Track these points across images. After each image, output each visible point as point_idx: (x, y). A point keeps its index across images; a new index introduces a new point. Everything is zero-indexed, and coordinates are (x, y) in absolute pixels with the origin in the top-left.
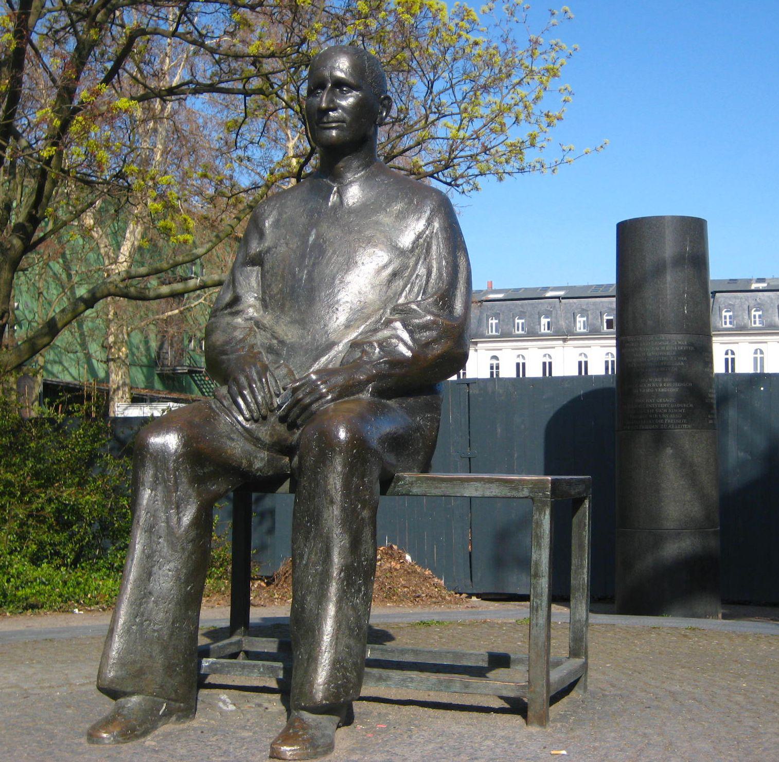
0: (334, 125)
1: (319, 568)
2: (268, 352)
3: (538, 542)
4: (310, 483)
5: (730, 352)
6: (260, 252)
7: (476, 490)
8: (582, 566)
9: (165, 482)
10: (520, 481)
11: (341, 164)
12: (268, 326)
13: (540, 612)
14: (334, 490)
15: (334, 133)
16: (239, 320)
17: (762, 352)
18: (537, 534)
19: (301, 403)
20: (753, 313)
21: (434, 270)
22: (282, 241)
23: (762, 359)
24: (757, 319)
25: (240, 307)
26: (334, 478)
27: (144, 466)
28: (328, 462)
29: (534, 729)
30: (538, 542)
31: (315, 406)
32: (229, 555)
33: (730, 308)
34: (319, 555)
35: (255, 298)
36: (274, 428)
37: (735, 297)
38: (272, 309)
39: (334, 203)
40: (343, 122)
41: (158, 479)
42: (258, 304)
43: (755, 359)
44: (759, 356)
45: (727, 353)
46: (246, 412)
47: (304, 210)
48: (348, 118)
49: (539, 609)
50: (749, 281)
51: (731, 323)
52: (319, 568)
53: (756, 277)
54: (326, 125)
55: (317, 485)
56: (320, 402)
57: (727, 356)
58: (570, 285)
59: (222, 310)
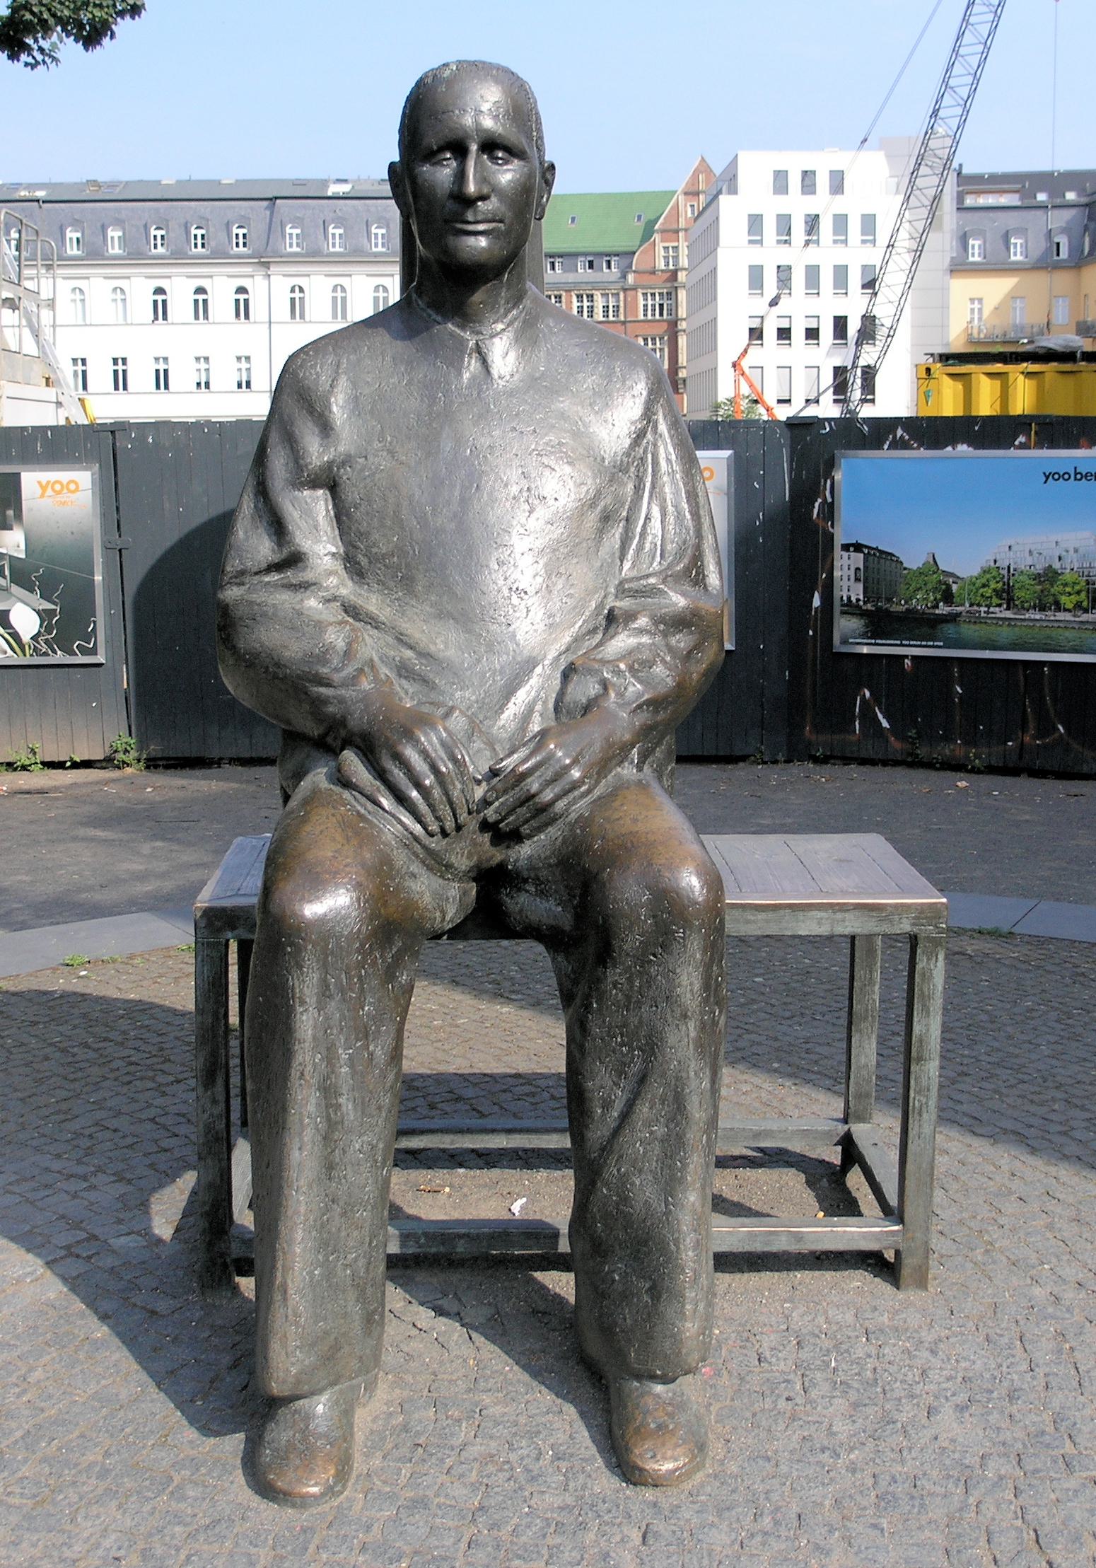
0: (481, 227)
1: (659, 1130)
2: (400, 676)
3: (924, 1005)
4: (630, 980)
5: (297, 289)
6: (330, 464)
7: (819, 923)
8: (871, 982)
9: (343, 992)
10: (896, 906)
11: (478, 297)
12: (382, 618)
13: (925, 1115)
14: (689, 995)
15: (483, 242)
16: (312, 603)
17: (343, 289)
18: (923, 993)
19: (537, 800)
20: (331, 230)
21: (670, 509)
22: (376, 445)
23: (344, 299)
24: (337, 241)
25: (308, 576)
26: (689, 974)
27: (300, 967)
28: (675, 946)
29: (909, 1295)
30: (924, 1005)
31: (560, 805)
32: (192, 969)
33: (297, 222)
34: (659, 1106)
35: (333, 555)
36: (474, 844)
37: (304, 207)
38: (379, 582)
39: (473, 378)
40: (501, 221)
41: (327, 987)
42: (338, 566)
43: (334, 299)
44: (339, 294)
45: (293, 291)
46: (429, 818)
47: (410, 383)
48: (509, 215)
49: (924, 1110)
50: (325, 183)
51: (298, 245)
52: (659, 1130)
53: (334, 177)
54: (471, 228)
55: (649, 983)
56: (571, 796)
57: (293, 295)
58: (53, 181)
59: (256, 573)
